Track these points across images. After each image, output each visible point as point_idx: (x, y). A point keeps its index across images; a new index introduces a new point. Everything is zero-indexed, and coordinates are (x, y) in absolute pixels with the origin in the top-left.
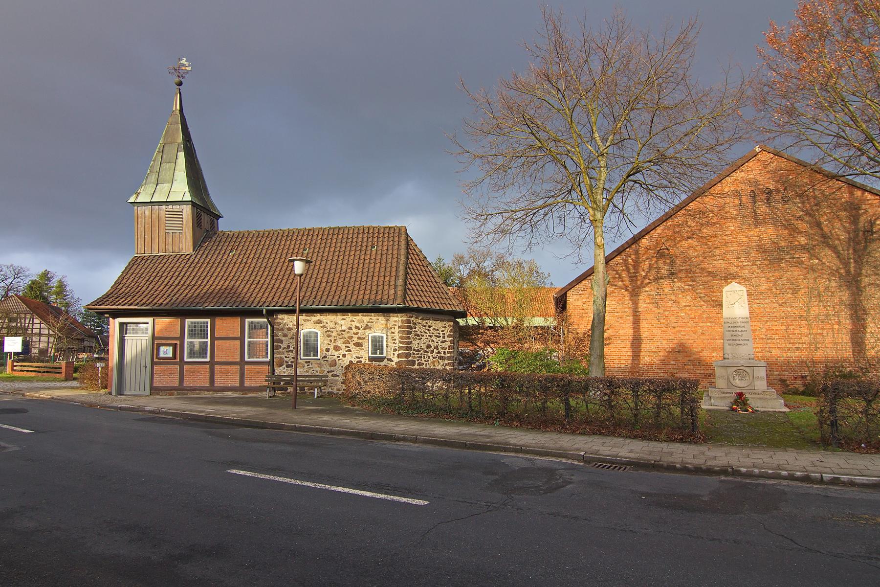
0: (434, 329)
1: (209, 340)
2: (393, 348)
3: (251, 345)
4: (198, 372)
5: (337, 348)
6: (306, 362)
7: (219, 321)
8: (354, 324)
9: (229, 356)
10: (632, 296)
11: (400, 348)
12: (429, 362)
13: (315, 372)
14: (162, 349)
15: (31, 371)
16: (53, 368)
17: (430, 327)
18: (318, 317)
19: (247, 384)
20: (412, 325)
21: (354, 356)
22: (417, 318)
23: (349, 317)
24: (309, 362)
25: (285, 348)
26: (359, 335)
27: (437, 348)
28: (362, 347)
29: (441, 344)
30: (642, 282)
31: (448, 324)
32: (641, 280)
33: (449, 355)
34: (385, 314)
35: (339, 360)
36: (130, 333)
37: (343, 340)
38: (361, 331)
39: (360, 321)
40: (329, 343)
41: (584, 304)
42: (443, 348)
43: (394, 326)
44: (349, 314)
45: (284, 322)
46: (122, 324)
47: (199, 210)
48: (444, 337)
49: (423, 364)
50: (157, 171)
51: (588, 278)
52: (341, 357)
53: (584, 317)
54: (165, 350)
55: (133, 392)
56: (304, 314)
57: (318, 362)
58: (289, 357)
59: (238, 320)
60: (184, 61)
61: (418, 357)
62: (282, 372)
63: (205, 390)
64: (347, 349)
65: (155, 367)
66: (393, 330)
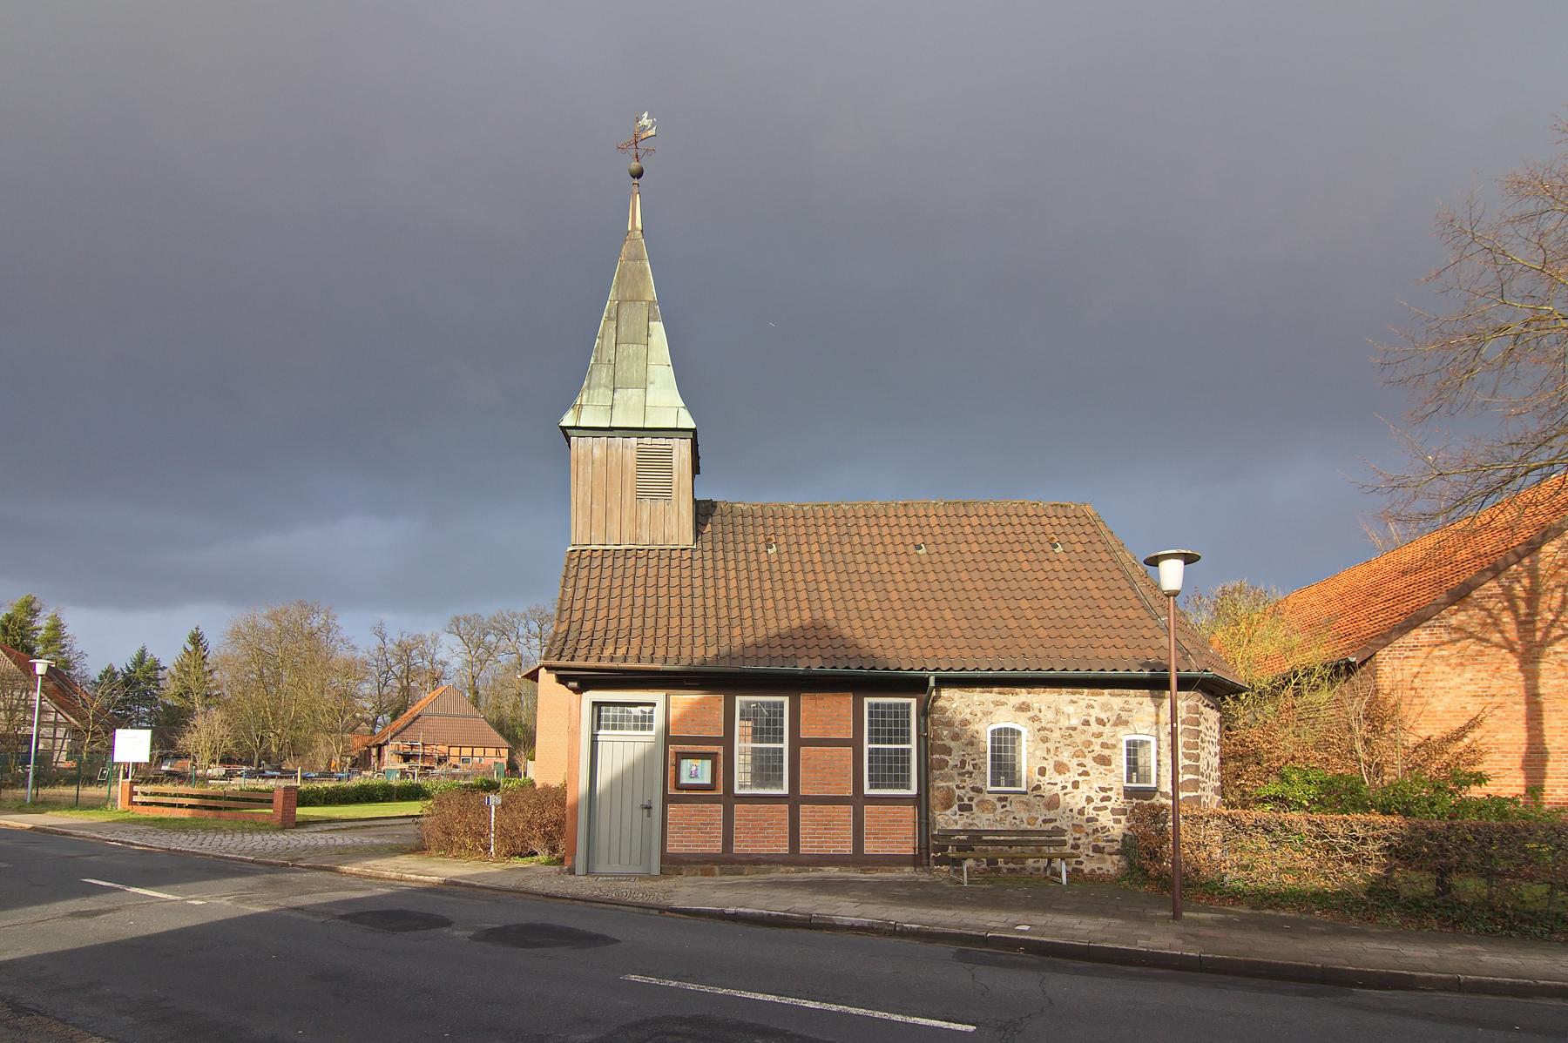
1: (785, 746)
3: (714, 756)
4: (766, 820)
5: (1060, 768)
6: (1000, 799)
7: (807, 702)
8: (1096, 712)
9: (829, 784)
10: (1526, 663)
13: (1018, 822)
14: (686, 765)
15: (181, 806)
16: (175, 795)
18: (1023, 695)
19: (870, 848)
21: (1096, 786)
23: (1085, 696)
24: (1005, 799)
25: (956, 766)
26: (1104, 739)
28: (1110, 765)
30: (1547, 634)
32: (1544, 630)
35: (1065, 794)
36: (607, 728)
38: (1107, 730)
41: (1415, 677)
44: (1086, 691)
45: (954, 706)
50: (609, 361)
51: (1424, 625)
53: (1416, 705)
54: (694, 768)
55: (616, 868)
56: (996, 690)
57: (1024, 798)
58: (964, 788)
59: (848, 700)
60: (645, 121)
62: (952, 822)
63: (779, 863)
64: (1081, 769)
65: (671, 808)
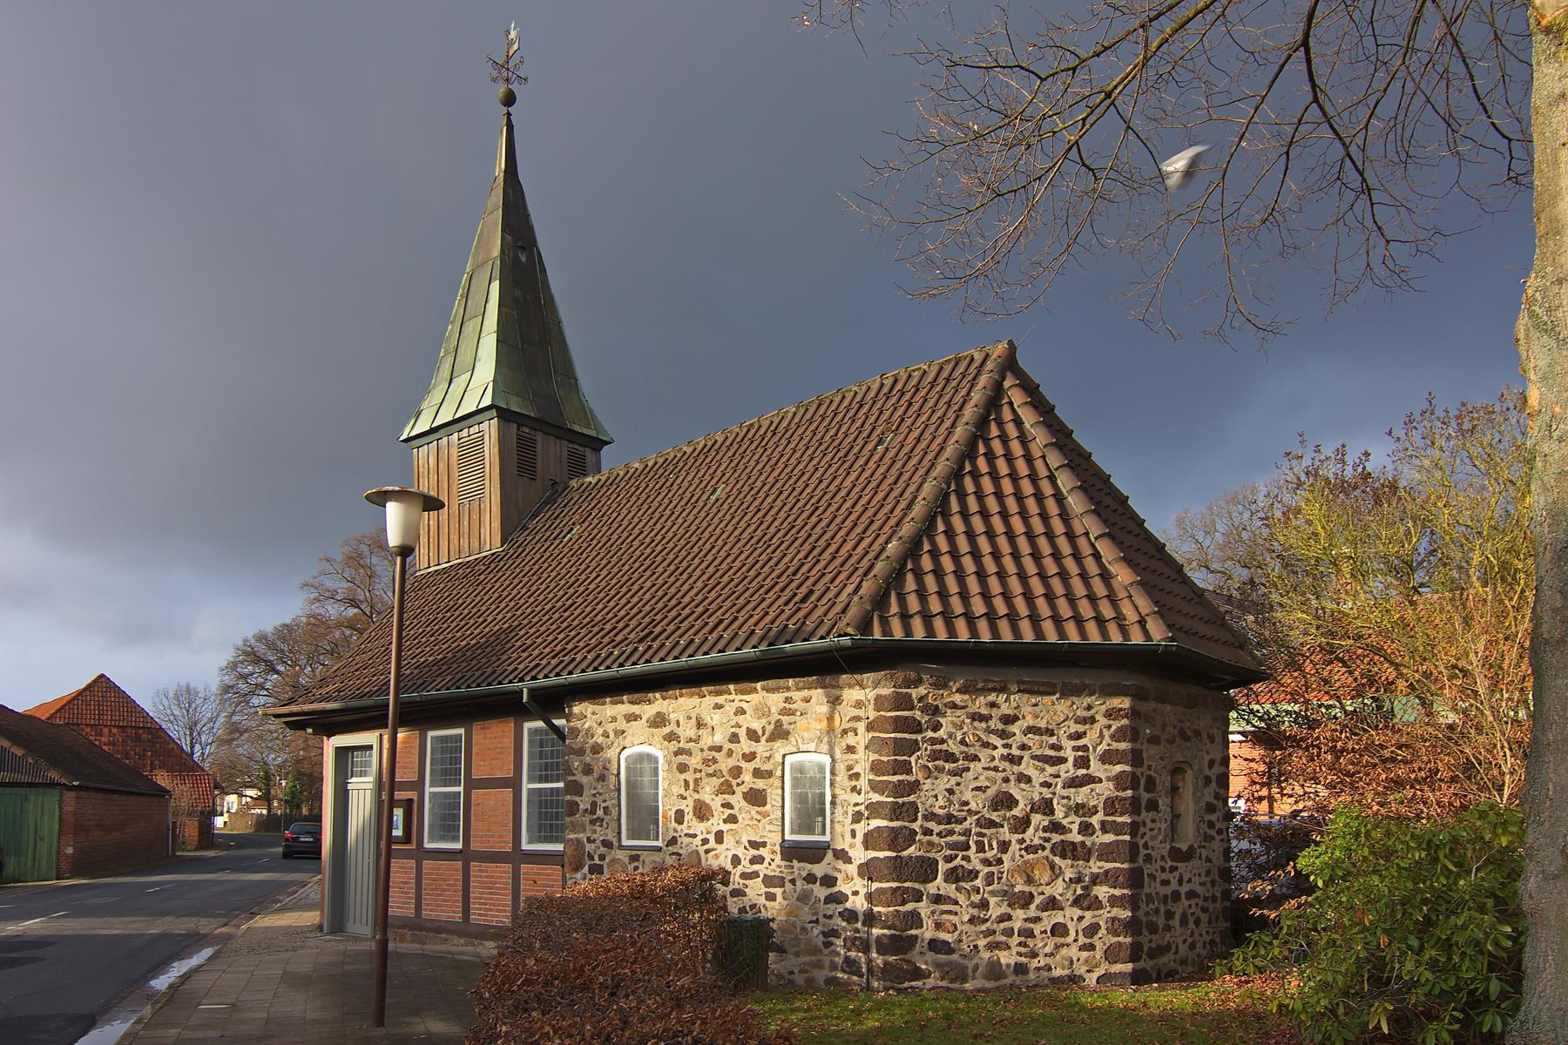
0: (1031, 730)
2: (851, 810)
11: (875, 811)
12: (1007, 865)
17: (1009, 720)
18: (659, 704)
20: (917, 714)
21: (744, 840)
22: (941, 684)
27: (1046, 807)
29: (1065, 792)
31: (1100, 706)
33: (1109, 838)
34: (828, 679)
35: (707, 852)
37: (716, 782)
39: (763, 712)
40: (682, 791)
42: (1079, 809)
43: (852, 724)
44: (731, 687)
46: (342, 752)
47: (527, 430)
48: (1083, 762)
49: (973, 874)
52: (712, 844)
61: (952, 846)
66: (850, 739)
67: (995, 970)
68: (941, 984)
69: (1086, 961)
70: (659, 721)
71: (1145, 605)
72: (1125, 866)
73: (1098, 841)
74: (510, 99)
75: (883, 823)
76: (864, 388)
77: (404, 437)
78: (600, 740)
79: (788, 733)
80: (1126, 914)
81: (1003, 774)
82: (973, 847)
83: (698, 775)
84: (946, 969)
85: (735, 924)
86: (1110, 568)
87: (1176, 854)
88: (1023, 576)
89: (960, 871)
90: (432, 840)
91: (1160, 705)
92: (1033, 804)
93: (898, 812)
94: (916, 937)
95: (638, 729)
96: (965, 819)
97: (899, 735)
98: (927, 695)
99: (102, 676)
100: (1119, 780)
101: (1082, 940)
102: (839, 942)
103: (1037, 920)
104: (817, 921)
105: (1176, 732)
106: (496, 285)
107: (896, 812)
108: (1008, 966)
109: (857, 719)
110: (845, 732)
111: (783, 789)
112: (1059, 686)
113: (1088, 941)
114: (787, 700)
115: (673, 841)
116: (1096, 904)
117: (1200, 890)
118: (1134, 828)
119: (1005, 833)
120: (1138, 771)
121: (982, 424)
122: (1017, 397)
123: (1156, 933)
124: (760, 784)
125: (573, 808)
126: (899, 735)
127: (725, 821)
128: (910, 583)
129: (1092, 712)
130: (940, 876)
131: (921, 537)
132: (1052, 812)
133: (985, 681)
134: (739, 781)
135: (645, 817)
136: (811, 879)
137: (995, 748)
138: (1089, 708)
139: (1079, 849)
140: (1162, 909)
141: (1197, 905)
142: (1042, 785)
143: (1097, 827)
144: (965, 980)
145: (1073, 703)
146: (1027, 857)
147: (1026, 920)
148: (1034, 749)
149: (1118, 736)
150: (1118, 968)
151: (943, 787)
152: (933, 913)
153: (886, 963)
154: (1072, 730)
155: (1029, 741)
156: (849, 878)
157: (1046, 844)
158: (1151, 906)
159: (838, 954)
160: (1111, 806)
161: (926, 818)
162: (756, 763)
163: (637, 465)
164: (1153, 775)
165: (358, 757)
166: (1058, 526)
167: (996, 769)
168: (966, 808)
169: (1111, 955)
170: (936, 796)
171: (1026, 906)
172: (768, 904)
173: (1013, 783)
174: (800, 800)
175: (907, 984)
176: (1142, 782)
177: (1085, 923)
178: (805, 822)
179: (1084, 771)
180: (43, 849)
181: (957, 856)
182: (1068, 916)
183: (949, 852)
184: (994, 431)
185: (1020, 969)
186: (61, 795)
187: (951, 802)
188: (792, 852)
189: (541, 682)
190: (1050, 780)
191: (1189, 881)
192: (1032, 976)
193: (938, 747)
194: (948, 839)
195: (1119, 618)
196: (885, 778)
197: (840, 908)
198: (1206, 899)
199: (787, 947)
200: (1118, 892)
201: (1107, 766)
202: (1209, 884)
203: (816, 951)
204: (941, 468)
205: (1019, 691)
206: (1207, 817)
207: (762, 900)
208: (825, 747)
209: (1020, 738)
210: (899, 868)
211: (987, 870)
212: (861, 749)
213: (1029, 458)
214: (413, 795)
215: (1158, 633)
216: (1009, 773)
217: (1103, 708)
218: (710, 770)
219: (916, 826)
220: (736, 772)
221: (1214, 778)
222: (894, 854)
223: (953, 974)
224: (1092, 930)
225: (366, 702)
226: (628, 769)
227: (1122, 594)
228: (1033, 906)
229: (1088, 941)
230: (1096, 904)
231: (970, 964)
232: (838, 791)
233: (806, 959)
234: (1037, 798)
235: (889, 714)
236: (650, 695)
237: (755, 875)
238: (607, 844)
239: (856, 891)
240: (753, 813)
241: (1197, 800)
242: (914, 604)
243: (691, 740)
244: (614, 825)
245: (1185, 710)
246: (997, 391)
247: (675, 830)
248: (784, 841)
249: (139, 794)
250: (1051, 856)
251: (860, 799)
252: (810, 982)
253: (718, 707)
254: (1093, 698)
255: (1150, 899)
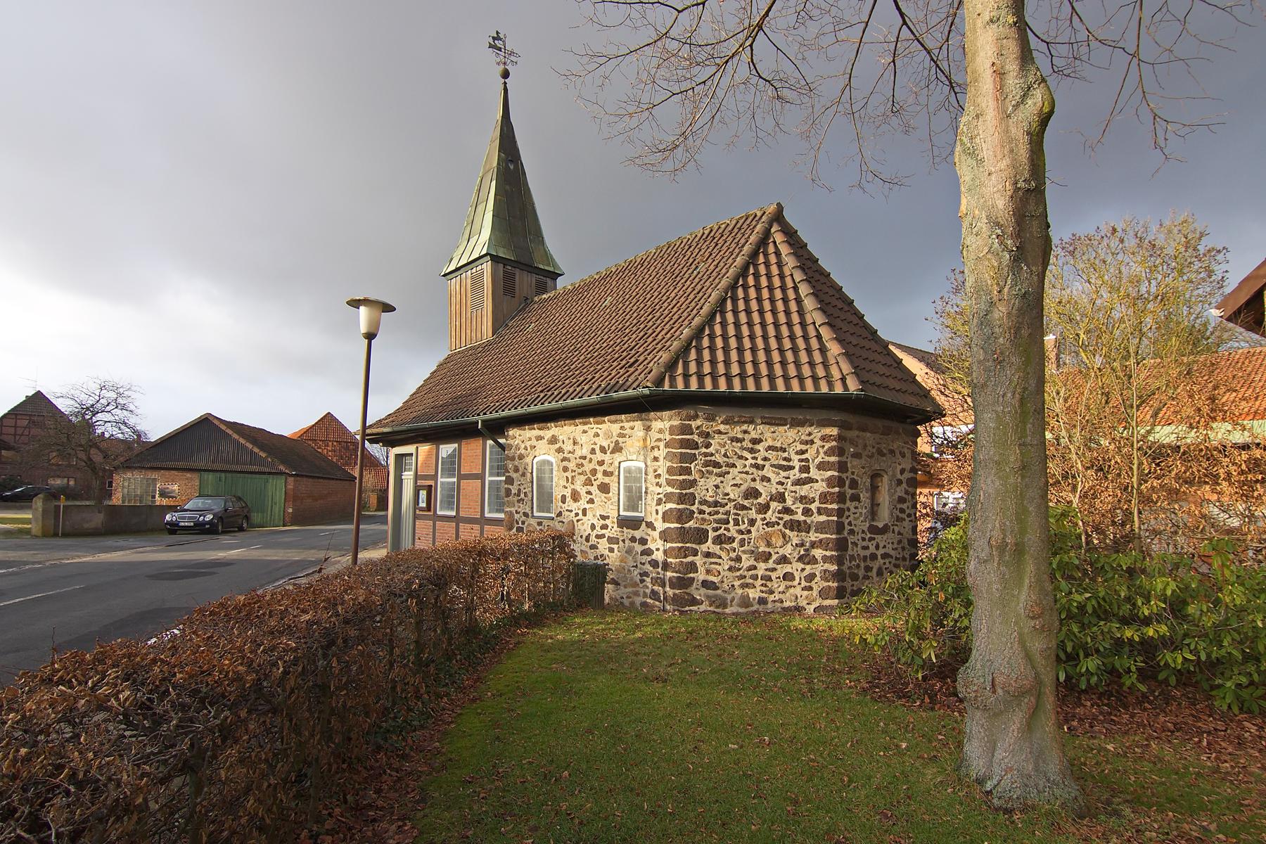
0: (770, 448)
2: (656, 497)
11: (669, 497)
12: (754, 534)
17: (756, 441)
18: (553, 430)
20: (696, 437)
22: (711, 418)
27: (781, 498)
29: (793, 488)
31: (817, 433)
33: (823, 518)
35: (578, 521)
39: (608, 435)
40: (565, 484)
42: (803, 499)
43: (656, 443)
44: (591, 420)
46: (399, 458)
48: (806, 469)
49: (732, 540)
52: (580, 516)
61: (717, 521)
66: (656, 453)
67: (745, 602)
68: (709, 609)
69: (807, 597)
70: (553, 440)
71: (846, 367)
72: (834, 536)
73: (815, 520)
74: (506, 75)
75: (673, 506)
76: (693, 236)
77: (443, 274)
78: (523, 451)
79: (622, 448)
80: (834, 568)
81: (752, 476)
82: (732, 522)
83: (573, 474)
84: (713, 599)
85: (582, 567)
86: (827, 344)
87: (874, 530)
88: (767, 350)
89: (723, 537)
90: (441, 509)
91: (861, 433)
92: (772, 496)
93: (683, 499)
94: (694, 578)
95: (542, 445)
96: (727, 504)
97: (683, 451)
98: (702, 425)
99: (329, 413)
100: (830, 482)
101: (804, 584)
102: (648, 580)
103: (774, 570)
104: (636, 566)
105: (874, 450)
106: (494, 183)
107: (682, 499)
108: (754, 599)
109: (659, 440)
110: (653, 448)
111: (619, 483)
112: (789, 420)
113: (808, 584)
114: (622, 428)
115: (560, 514)
116: (813, 561)
117: (892, 553)
118: (840, 513)
119: (753, 514)
120: (844, 476)
121: (754, 255)
122: (779, 238)
123: (857, 580)
124: (607, 480)
125: (508, 492)
126: (683, 451)
127: (588, 502)
128: (693, 355)
129: (812, 437)
130: (710, 540)
131: (704, 326)
132: (784, 501)
133: (740, 417)
134: (595, 478)
135: (546, 499)
136: (633, 539)
137: (747, 459)
138: (810, 434)
139: (803, 525)
140: (862, 565)
141: (890, 563)
142: (777, 483)
143: (815, 511)
144: (725, 607)
145: (799, 431)
146: (767, 529)
147: (766, 570)
148: (772, 460)
149: (829, 452)
150: (828, 602)
151: (712, 484)
152: (705, 563)
153: (674, 594)
154: (798, 449)
155: (771, 454)
156: (654, 540)
157: (780, 521)
158: (853, 563)
159: (648, 587)
160: (824, 497)
161: (700, 503)
162: (604, 467)
163: (569, 287)
164: (856, 478)
165: (408, 459)
166: (795, 318)
167: (747, 473)
168: (727, 497)
169: (823, 594)
170: (707, 489)
171: (766, 560)
172: (610, 554)
173: (758, 481)
174: (629, 490)
175: (687, 608)
176: (847, 483)
177: (806, 573)
178: (633, 505)
179: (806, 475)
180: (276, 509)
181: (721, 528)
182: (795, 567)
183: (715, 525)
184: (761, 259)
185: (762, 601)
186: (286, 479)
187: (717, 494)
188: (624, 523)
189: (488, 416)
190: (783, 480)
191: (885, 547)
192: (770, 606)
193: (709, 458)
194: (715, 517)
195: (828, 377)
196: (675, 477)
197: (649, 559)
198: (897, 559)
199: (620, 582)
200: (828, 553)
201: (821, 472)
202: (900, 550)
203: (636, 585)
204: (724, 282)
205: (762, 423)
206: (899, 506)
207: (606, 552)
208: (642, 458)
209: (763, 453)
210: (683, 535)
211: (741, 537)
212: (661, 459)
213: (782, 276)
214: (431, 483)
215: (853, 386)
216: (755, 476)
217: (820, 435)
218: (580, 471)
219: (694, 508)
220: (594, 472)
221: (904, 481)
222: (680, 526)
223: (717, 603)
224: (811, 577)
225: (404, 428)
226: (537, 469)
227: (832, 361)
228: (771, 561)
229: (808, 584)
230: (813, 561)
231: (729, 597)
232: (649, 485)
233: (630, 590)
234: (774, 491)
235: (677, 437)
236: (549, 424)
237: (602, 536)
238: (526, 515)
239: (658, 547)
240: (603, 498)
241: (891, 495)
242: (693, 368)
243: (570, 452)
244: (529, 503)
245: (882, 436)
246: (767, 234)
247: (561, 507)
248: (619, 515)
249: (337, 479)
250: (783, 529)
251: (660, 490)
252: (632, 603)
253: (585, 432)
254: (813, 428)
255: (852, 558)
